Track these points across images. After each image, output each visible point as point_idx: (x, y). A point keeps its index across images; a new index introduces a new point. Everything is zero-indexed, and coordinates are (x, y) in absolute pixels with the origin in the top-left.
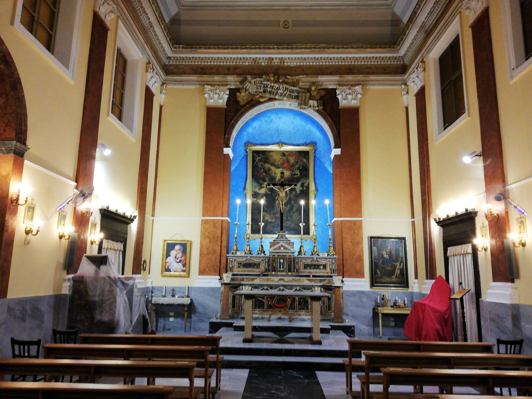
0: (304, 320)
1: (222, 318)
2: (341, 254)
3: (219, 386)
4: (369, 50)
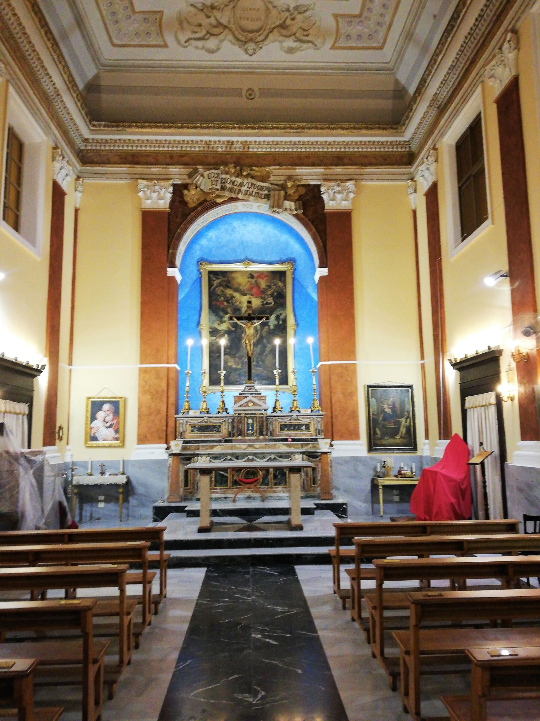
0: (279, 498)
1: (170, 500)
2: (329, 410)
3: (164, 593)
4: (363, 131)
